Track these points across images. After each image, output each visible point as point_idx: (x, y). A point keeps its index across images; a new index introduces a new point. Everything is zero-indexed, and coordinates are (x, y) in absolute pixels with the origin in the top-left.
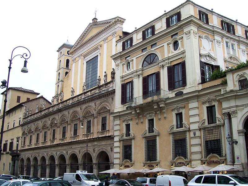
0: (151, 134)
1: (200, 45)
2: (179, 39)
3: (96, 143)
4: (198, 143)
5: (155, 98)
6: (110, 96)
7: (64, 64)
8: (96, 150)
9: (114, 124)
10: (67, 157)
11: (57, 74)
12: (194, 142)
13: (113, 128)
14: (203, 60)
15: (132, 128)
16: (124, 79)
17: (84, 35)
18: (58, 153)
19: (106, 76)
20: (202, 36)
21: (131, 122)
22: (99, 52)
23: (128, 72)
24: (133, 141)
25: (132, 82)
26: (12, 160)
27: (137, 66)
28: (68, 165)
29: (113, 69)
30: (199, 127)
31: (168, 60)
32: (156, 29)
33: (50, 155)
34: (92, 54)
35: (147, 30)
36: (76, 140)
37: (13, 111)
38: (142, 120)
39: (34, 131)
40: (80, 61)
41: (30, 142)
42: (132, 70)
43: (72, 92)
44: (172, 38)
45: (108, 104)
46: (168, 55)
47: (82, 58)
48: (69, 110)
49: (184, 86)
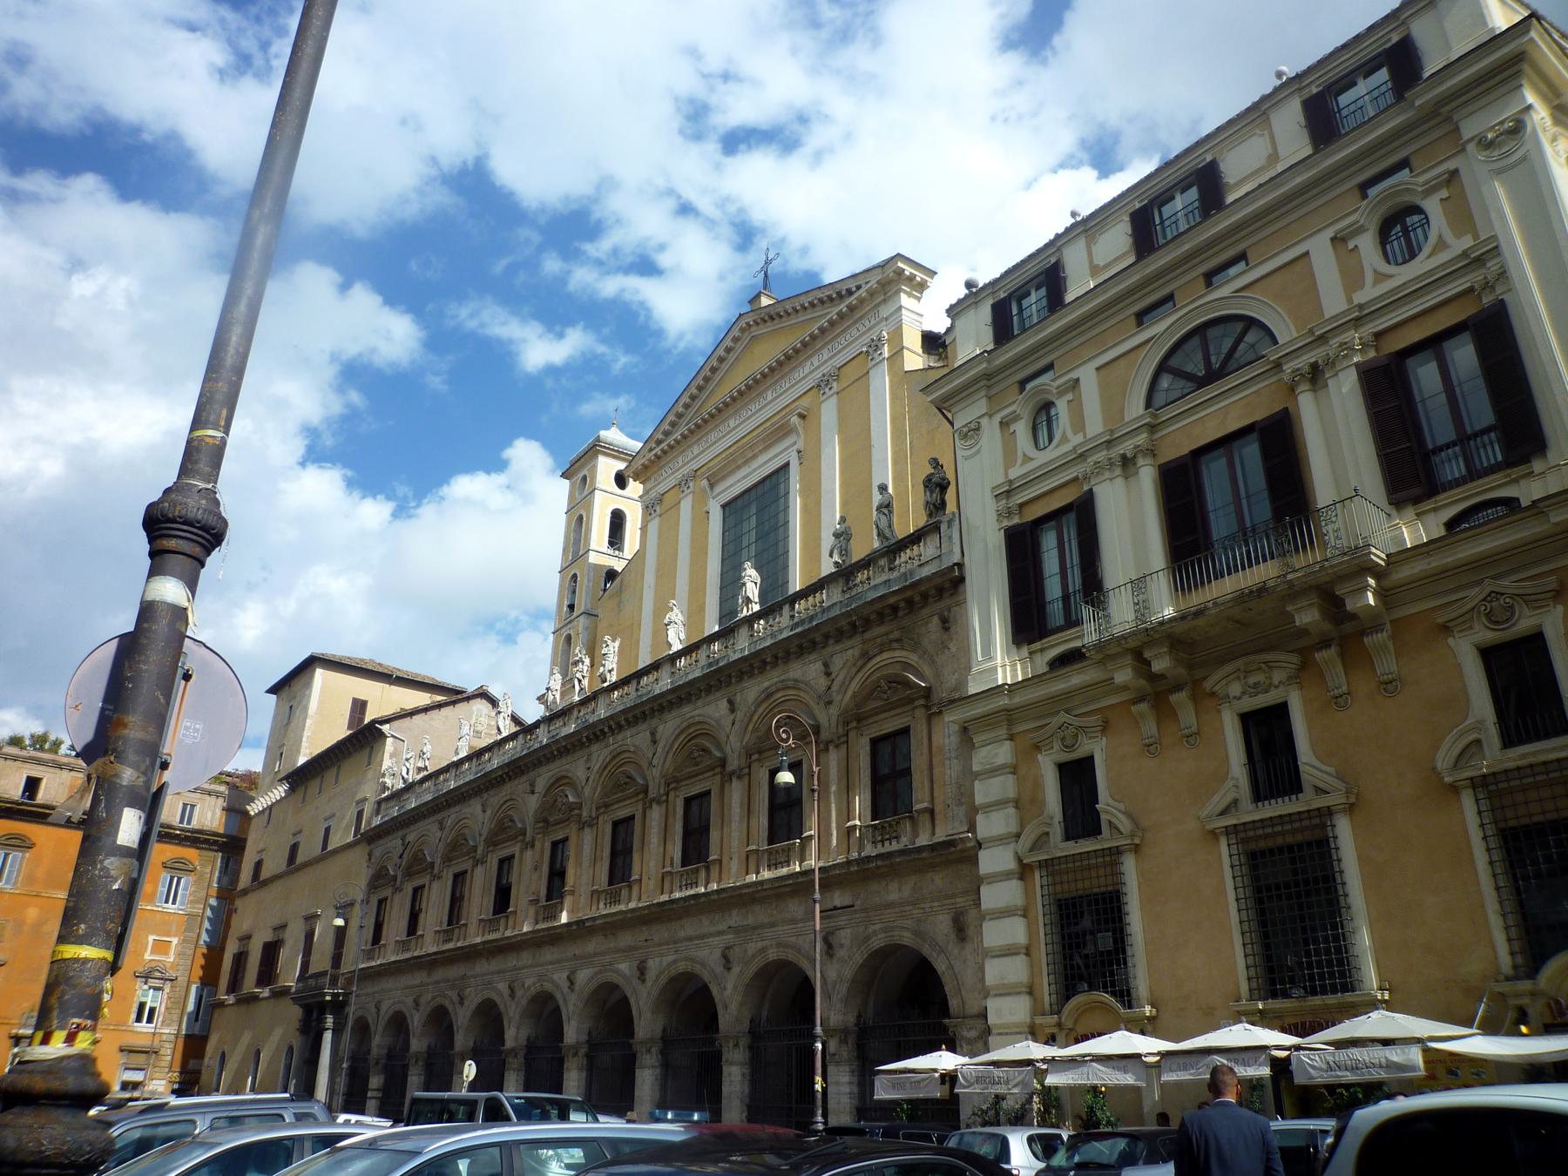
2: (1061, 394)
6: (926, 611)
8: (847, 942)
18: (583, 976)
21: (1097, 748)
22: (795, 448)
25: (1083, 513)
27: (1112, 403)
28: (575, 1049)
31: (1008, 498)
33: (533, 991)
35: (1165, 198)
37: (328, 768)
41: (412, 928)
42: (1067, 438)
45: (913, 658)
48: (654, 722)
49: (1526, 460)
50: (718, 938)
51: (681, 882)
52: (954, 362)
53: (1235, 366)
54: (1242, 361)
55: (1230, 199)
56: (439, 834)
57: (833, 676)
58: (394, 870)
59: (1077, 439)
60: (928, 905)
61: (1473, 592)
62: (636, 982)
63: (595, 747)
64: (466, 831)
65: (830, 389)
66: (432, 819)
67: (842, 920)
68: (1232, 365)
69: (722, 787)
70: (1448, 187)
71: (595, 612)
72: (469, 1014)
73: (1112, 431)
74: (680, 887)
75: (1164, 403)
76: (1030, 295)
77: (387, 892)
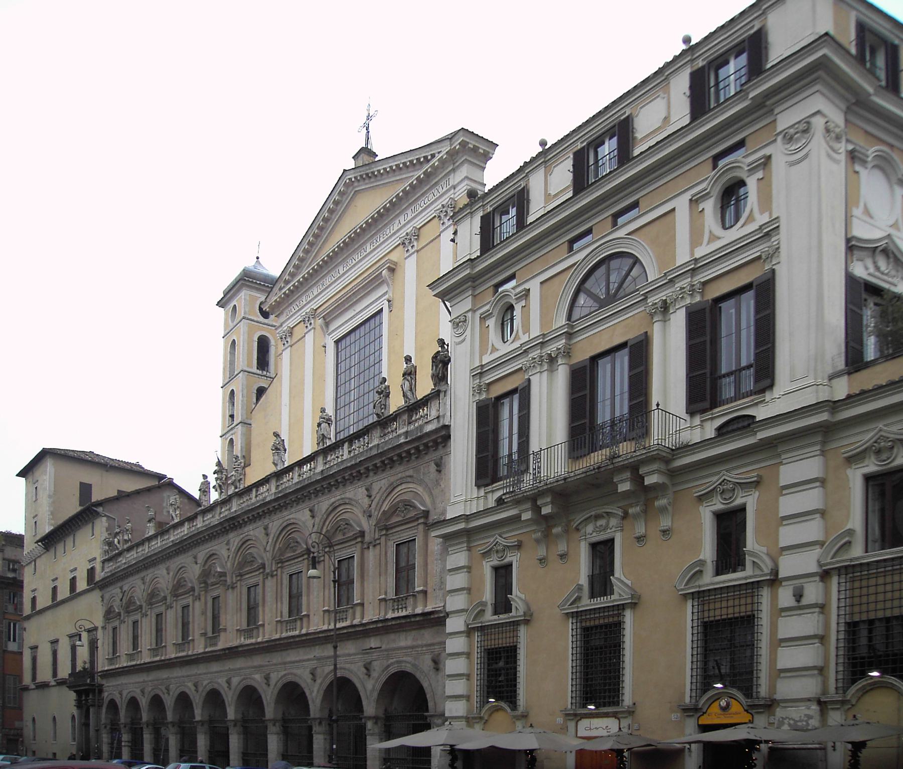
0: (601, 602)
1: (851, 198)
2: (752, 171)
3: (373, 642)
4: (812, 634)
5: (625, 449)
6: (427, 458)
7: (247, 356)
9: (445, 566)
10: (269, 696)
11: (224, 399)
12: (792, 626)
13: (442, 583)
14: (860, 270)
15: (518, 580)
16: (488, 379)
17: (321, 228)
19: (410, 374)
20: (863, 151)
21: (513, 558)
22: (386, 297)
23: (504, 349)
24: (523, 631)
25: (524, 393)
26: (79, 705)
29: (441, 342)
30: (820, 565)
32: (639, 135)
34: (359, 307)
36: (297, 633)
38: (562, 547)
39: (144, 605)
40: (309, 338)
41: (135, 645)
43: (277, 449)
44: (715, 167)
45: (420, 490)
46: (692, 254)
47: (318, 328)
49: (762, 391)
50: (308, 663)
51: (287, 627)
52: (766, 65)
53: (622, 294)
54: (628, 291)
55: (636, 152)
56: (142, 587)
57: (373, 497)
58: (119, 609)
59: (524, 338)
60: (420, 649)
61: (715, 479)
62: (265, 686)
63: (231, 535)
64: (158, 586)
65: (412, 247)
66: (137, 576)
67: (375, 656)
68: (621, 293)
69: (362, 554)
70: (764, 169)
71: (249, 422)
72: (174, 700)
73: (544, 335)
74: (287, 630)
75: (579, 317)
76: (604, 143)
77: (117, 623)
